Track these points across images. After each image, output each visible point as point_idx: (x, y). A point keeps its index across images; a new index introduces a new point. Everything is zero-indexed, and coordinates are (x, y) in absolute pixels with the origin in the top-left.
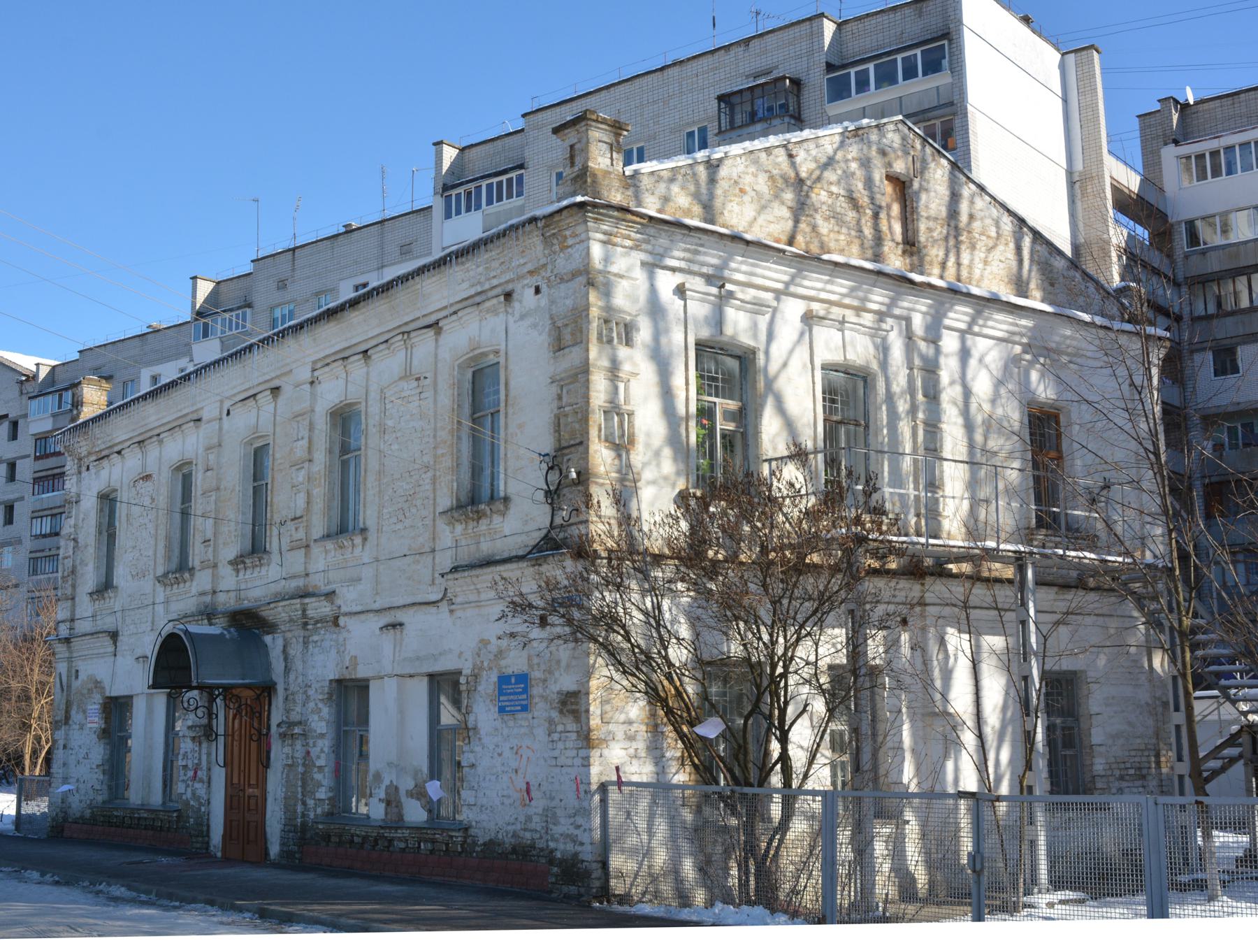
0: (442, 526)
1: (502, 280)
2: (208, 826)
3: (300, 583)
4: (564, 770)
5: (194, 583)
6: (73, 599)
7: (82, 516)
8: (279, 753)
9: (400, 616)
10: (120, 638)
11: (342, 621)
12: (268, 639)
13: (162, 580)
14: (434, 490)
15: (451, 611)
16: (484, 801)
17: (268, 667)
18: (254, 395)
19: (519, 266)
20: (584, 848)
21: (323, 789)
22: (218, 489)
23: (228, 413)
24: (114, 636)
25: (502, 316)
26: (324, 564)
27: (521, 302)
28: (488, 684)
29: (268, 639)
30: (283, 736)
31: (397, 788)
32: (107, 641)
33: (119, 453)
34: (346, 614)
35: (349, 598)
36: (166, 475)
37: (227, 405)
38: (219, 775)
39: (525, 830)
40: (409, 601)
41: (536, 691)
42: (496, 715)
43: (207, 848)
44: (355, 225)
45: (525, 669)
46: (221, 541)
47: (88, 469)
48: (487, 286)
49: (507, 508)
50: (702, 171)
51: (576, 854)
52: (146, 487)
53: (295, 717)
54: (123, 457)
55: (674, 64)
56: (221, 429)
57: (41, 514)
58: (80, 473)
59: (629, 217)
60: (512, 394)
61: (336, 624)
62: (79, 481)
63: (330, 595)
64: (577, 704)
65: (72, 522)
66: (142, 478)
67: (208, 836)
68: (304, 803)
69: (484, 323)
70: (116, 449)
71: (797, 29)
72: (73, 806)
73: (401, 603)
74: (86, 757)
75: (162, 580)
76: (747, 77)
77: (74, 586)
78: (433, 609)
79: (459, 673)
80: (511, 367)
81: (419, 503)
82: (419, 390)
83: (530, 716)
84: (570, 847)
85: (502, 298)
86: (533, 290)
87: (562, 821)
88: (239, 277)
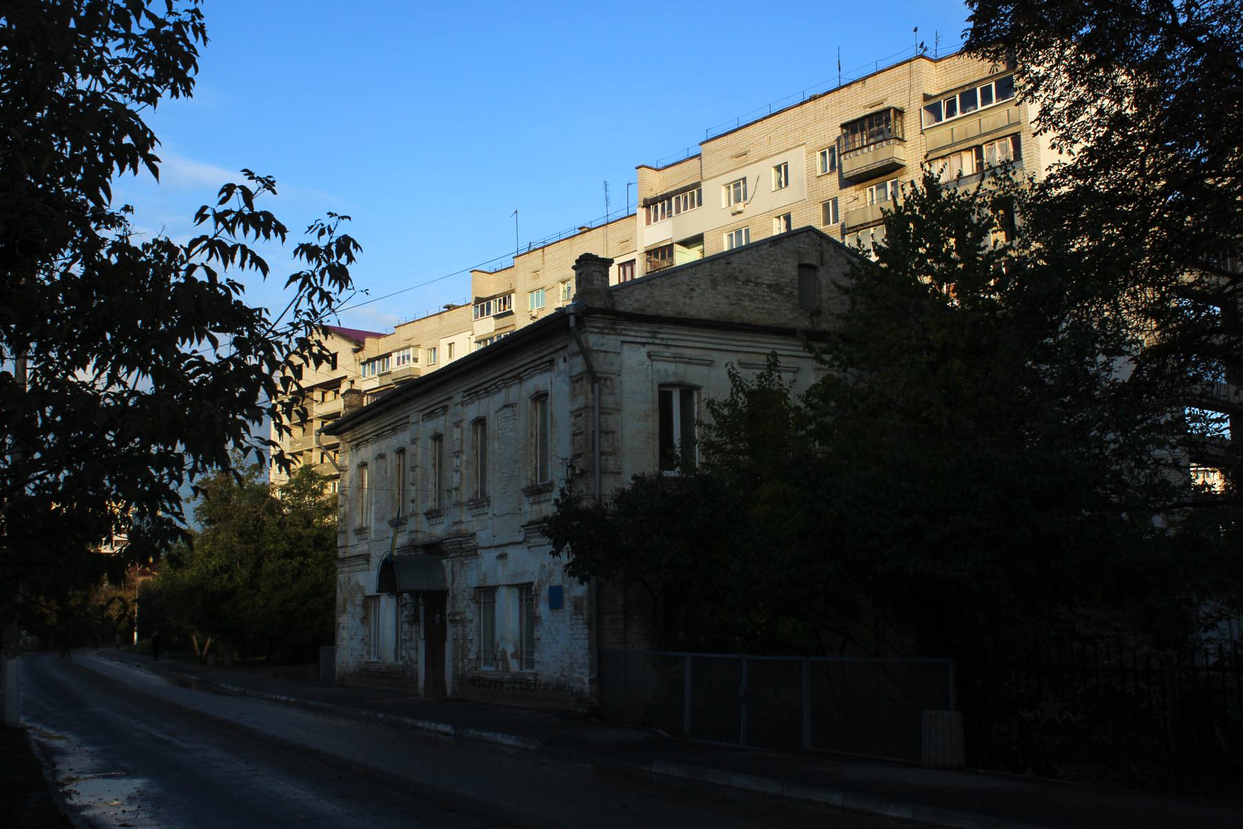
8: (450, 631)
12: (444, 561)
17: (445, 580)
26: (469, 521)
28: (544, 593)
29: (444, 561)
30: (451, 621)
35: (483, 538)
38: (422, 644)
40: (510, 540)
41: (566, 595)
50: (392, 457)
55: (864, 79)
57: (958, 148)
71: (900, 68)
74: (356, 634)
76: (865, 107)
79: (532, 583)
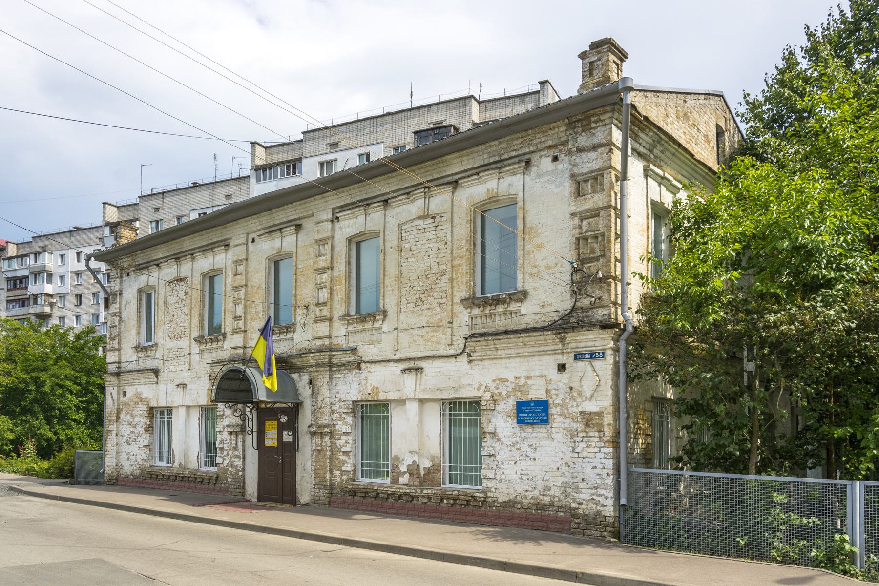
0: (458, 308)
1: (520, 152)
2: (244, 483)
4: (586, 460)
5: (226, 342)
6: (119, 350)
7: (124, 303)
9: (418, 364)
10: (161, 373)
11: (363, 366)
13: (200, 340)
14: (452, 287)
15: (470, 362)
16: (503, 477)
18: (281, 229)
19: (540, 142)
20: (606, 509)
21: (349, 465)
22: (246, 286)
23: (253, 241)
24: (156, 372)
25: (519, 177)
27: (538, 166)
31: (418, 466)
32: (152, 375)
33: (158, 265)
34: (365, 363)
36: (197, 279)
37: (251, 237)
39: (543, 495)
42: (515, 425)
43: (243, 495)
44: (200, 182)
45: (544, 397)
46: (249, 318)
47: (128, 275)
48: (505, 156)
51: (599, 512)
52: (181, 288)
53: (324, 420)
54: (160, 268)
56: (247, 250)
58: (121, 277)
59: (506, 163)
60: (528, 225)
61: (360, 369)
62: (121, 283)
63: (354, 350)
64: (601, 420)
65: (117, 306)
66: (177, 281)
68: (331, 472)
69: (501, 181)
70: (156, 262)
72: (125, 468)
73: (420, 355)
75: (200, 340)
77: (119, 343)
78: (453, 360)
80: (527, 208)
81: (436, 294)
82: (434, 225)
83: (549, 427)
84: (594, 508)
85: (524, 164)
86: (550, 159)
87: (584, 491)
88: (129, 205)
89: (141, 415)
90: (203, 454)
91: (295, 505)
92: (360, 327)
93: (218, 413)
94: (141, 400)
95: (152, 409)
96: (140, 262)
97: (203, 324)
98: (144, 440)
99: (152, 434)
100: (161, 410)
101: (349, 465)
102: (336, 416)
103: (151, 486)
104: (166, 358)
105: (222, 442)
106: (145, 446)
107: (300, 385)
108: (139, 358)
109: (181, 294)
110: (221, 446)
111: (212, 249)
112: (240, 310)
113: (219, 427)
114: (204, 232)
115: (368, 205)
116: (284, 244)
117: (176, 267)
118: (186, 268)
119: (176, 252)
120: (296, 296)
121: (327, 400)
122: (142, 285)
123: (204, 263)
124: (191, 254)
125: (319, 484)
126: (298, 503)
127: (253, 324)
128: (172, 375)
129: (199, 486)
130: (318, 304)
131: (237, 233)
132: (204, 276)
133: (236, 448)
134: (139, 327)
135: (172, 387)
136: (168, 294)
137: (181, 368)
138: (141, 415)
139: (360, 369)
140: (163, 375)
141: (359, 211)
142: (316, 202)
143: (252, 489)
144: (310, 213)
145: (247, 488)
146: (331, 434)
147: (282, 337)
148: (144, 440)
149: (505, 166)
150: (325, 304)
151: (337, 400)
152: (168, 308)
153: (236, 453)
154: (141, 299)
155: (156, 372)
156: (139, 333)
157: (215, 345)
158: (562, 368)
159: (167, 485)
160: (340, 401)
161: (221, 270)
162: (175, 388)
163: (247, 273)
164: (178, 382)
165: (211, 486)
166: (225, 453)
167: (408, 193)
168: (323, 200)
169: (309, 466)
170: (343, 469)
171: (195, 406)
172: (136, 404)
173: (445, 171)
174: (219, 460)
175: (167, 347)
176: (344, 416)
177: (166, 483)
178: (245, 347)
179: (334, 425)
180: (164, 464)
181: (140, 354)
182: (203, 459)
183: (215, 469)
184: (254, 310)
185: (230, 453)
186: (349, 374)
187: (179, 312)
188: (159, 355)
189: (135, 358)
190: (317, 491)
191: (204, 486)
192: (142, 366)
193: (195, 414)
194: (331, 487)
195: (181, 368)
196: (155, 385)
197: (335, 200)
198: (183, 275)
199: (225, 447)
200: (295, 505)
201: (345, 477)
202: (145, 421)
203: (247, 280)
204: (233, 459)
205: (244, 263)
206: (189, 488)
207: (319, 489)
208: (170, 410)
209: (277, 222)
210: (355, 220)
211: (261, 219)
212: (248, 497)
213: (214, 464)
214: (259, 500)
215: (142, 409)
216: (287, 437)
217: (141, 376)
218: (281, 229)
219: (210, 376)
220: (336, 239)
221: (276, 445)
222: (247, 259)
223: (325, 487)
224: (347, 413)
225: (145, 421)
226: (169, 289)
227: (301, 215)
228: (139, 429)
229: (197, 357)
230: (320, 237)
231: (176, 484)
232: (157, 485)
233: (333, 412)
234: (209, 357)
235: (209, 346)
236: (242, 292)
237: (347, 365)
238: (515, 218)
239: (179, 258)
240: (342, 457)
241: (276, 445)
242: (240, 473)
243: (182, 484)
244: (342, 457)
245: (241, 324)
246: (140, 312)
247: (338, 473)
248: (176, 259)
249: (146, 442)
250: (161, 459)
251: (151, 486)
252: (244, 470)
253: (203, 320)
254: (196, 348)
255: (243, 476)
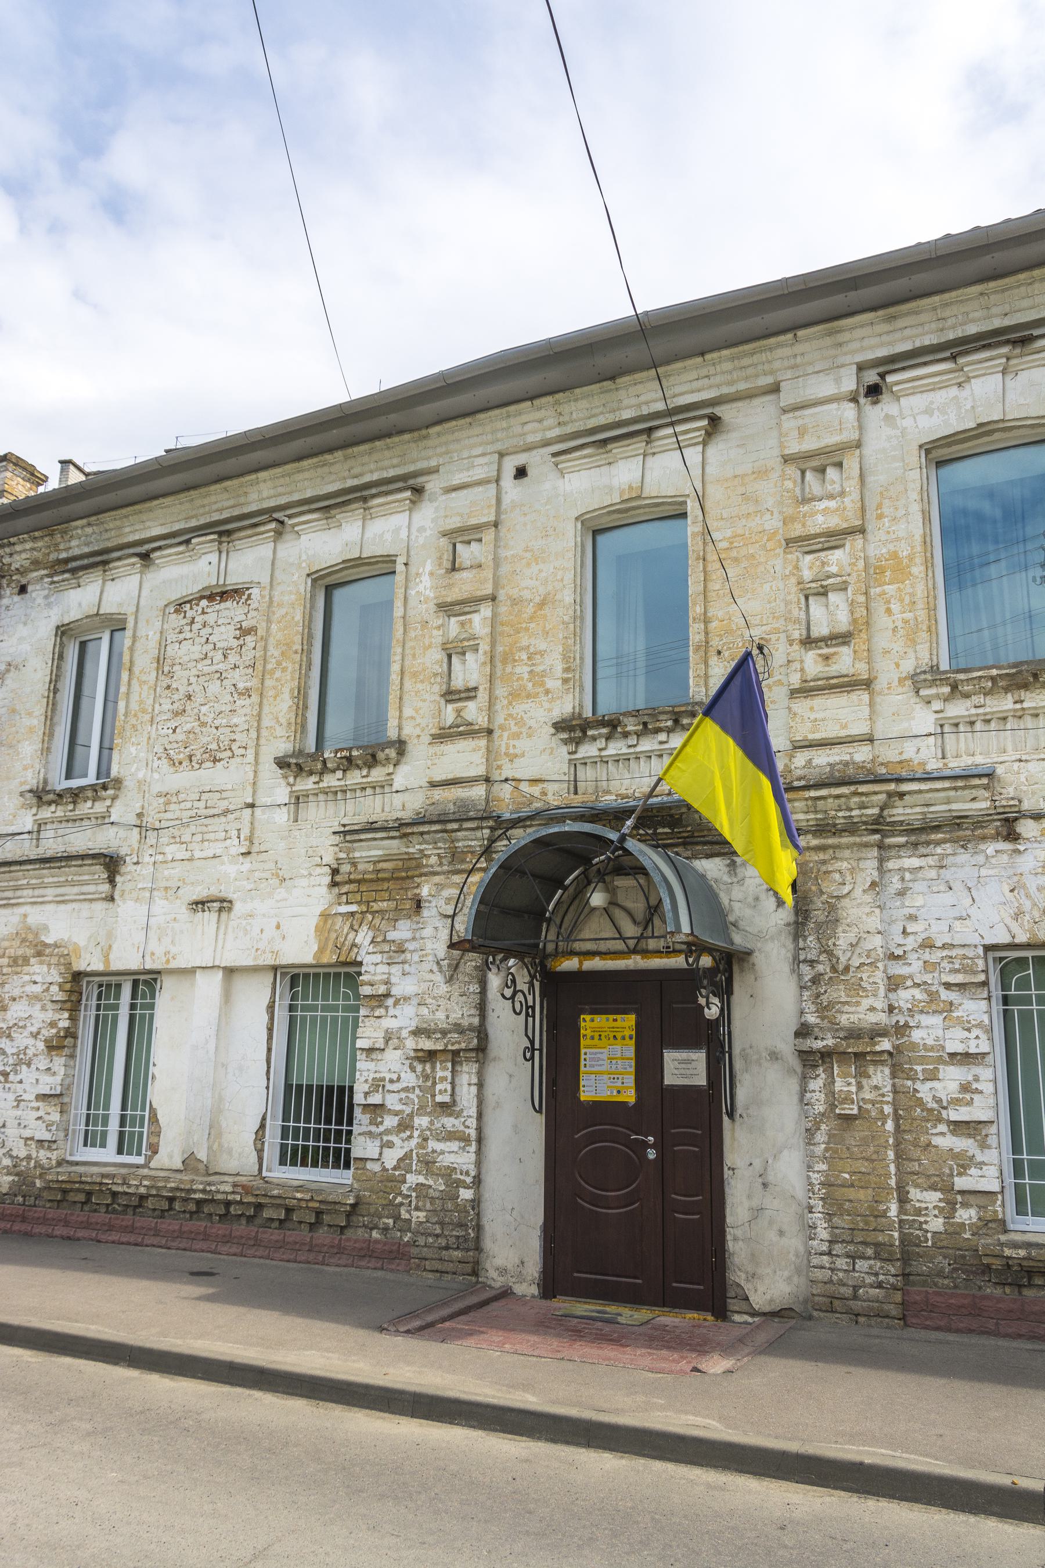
2: (479, 1228)
3: (862, 754)
5: (403, 770)
10: (128, 868)
11: (1027, 828)
22: (494, 598)
23: (521, 473)
24: (111, 864)
46: (501, 691)
49: (401, 753)
53: (865, 1011)
61: (1012, 836)
66: (211, 598)
67: (478, 1249)
68: (903, 1200)
75: (291, 765)
89: (34, 998)
90: (274, 1126)
91: (721, 1313)
92: (1006, 703)
93: (365, 990)
94: (41, 950)
95: (77, 976)
96: (77, 552)
97: (304, 718)
98: (44, 1075)
99: (72, 1056)
100: (108, 985)
101: (992, 1171)
102: (904, 997)
103: (59, 1231)
104: (150, 820)
105: (378, 1084)
106: (43, 1097)
107: (737, 893)
108: (40, 825)
109: (225, 636)
110: (375, 1099)
111: (365, 499)
112: (469, 671)
113: (369, 1034)
114: (339, 454)
115: (229, 533)
116: (369, 535)
117: (214, 557)
118: (247, 560)
119: (216, 517)
120: (706, 621)
121: (877, 941)
122: (74, 615)
123: (324, 544)
124: (276, 520)
125: (857, 1234)
126: (733, 1305)
127: (519, 708)
128: (174, 872)
129: (274, 1235)
130: (809, 642)
131: (464, 458)
132: (314, 581)
133: (447, 1108)
134: (49, 734)
135: (170, 910)
136: (172, 637)
137: (217, 848)
138: (34, 998)
139: (1012, 836)
140: (130, 877)
141: (205, 544)
142: (799, 348)
143: (514, 1243)
144: (769, 380)
145: (488, 1244)
146: (897, 1062)
147: (647, 745)
148: (44, 1075)
149: (374, 496)
150: (842, 638)
151: (911, 942)
152: (171, 675)
153: (450, 1122)
154: (61, 657)
155: (111, 864)
156: (46, 751)
157: (355, 777)
158: (257, 950)
159: (131, 1229)
160: (927, 945)
161: (390, 560)
162: (184, 913)
163: (497, 562)
164: (200, 892)
165: (323, 1235)
166: (390, 1122)
167: (183, 538)
168: (828, 341)
169: (791, 1171)
170: (961, 1183)
171: (255, 969)
172: (19, 962)
173: (428, 458)
174: (363, 1147)
175: (156, 788)
176: (945, 995)
177: (128, 1219)
178: (487, 780)
179: (902, 1030)
180: (107, 1154)
181: (46, 813)
182: (273, 1139)
183: (344, 1177)
184: (523, 670)
185: (422, 1121)
186: (963, 857)
187: (214, 687)
188: (122, 811)
189: (27, 822)
190: (842, 1263)
191: (292, 1236)
192: (51, 844)
193: (254, 1000)
194: (909, 1250)
195: (217, 848)
196: (100, 906)
197: (872, 339)
198: (233, 580)
199: (392, 1102)
200: (721, 1313)
201: (966, 1215)
202: (50, 1015)
203: (496, 584)
204: (432, 1144)
205: (488, 536)
206: (227, 1239)
207: (853, 1257)
208: (146, 983)
209: (627, 415)
210: (954, 391)
211: (566, 409)
212: (495, 1279)
213: (343, 1159)
214: (553, 1282)
215: (44, 976)
216: (684, 1067)
217: (49, 876)
218: (650, 430)
219: (335, 872)
220: (868, 450)
221: (630, 1097)
222: (496, 525)
223: (881, 1251)
224: (961, 986)
225: (50, 1015)
226: (176, 620)
227: (726, 390)
228: (22, 1040)
229: (282, 817)
230: (810, 444)
231: (170, 1224)
232: (87, 1225)
233: (894, 984)
234: (324, 819)
235: (331, 781)
236: (479, 621)
237: (959, 829)
238: (389, 604)
239: (229, 533)
240: (946, 1141)
241: (630, 1097)
242: (466, 1194)
243: (201, 1224)
244: (946, 1141)
245: (473, 711)
246: (56, 691)
247: (933, 1197)
248: (221, 534)
249: (49, 1084)
250: (89, 1140)
251: (59, 1231)
252: (478, 1181)
253: (306, 707)
254: (277, 789)
255: (476, 1203)
